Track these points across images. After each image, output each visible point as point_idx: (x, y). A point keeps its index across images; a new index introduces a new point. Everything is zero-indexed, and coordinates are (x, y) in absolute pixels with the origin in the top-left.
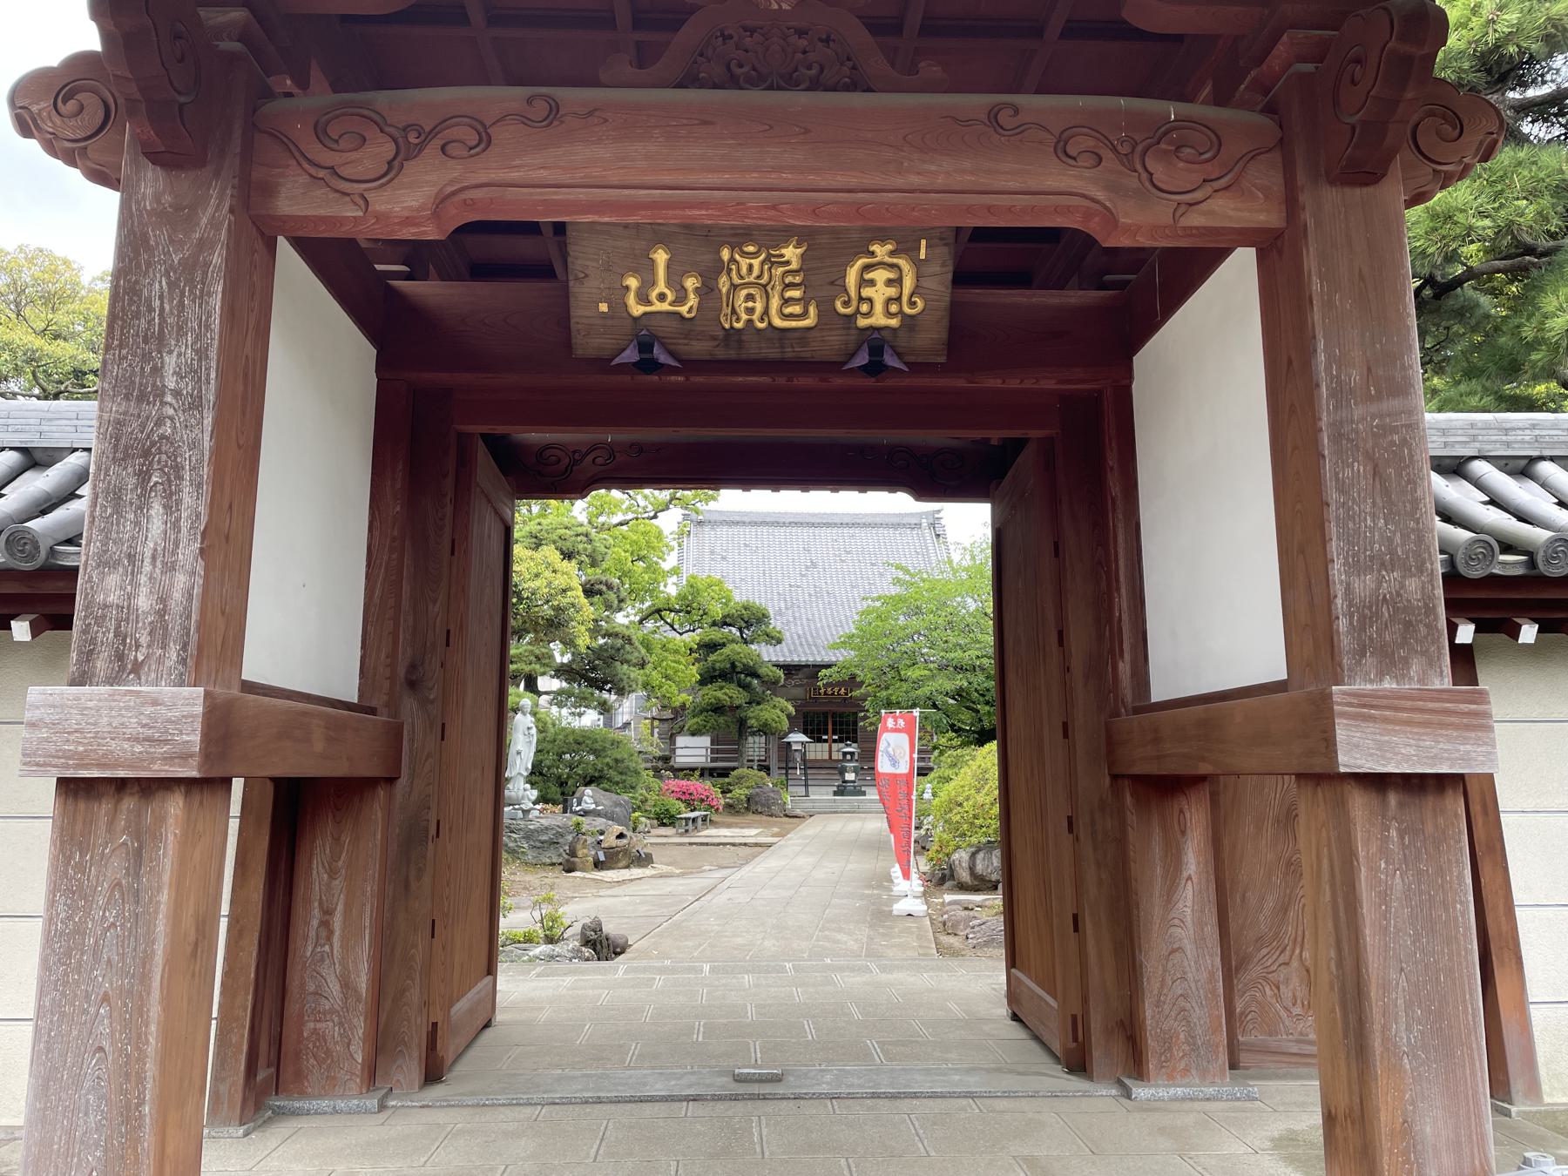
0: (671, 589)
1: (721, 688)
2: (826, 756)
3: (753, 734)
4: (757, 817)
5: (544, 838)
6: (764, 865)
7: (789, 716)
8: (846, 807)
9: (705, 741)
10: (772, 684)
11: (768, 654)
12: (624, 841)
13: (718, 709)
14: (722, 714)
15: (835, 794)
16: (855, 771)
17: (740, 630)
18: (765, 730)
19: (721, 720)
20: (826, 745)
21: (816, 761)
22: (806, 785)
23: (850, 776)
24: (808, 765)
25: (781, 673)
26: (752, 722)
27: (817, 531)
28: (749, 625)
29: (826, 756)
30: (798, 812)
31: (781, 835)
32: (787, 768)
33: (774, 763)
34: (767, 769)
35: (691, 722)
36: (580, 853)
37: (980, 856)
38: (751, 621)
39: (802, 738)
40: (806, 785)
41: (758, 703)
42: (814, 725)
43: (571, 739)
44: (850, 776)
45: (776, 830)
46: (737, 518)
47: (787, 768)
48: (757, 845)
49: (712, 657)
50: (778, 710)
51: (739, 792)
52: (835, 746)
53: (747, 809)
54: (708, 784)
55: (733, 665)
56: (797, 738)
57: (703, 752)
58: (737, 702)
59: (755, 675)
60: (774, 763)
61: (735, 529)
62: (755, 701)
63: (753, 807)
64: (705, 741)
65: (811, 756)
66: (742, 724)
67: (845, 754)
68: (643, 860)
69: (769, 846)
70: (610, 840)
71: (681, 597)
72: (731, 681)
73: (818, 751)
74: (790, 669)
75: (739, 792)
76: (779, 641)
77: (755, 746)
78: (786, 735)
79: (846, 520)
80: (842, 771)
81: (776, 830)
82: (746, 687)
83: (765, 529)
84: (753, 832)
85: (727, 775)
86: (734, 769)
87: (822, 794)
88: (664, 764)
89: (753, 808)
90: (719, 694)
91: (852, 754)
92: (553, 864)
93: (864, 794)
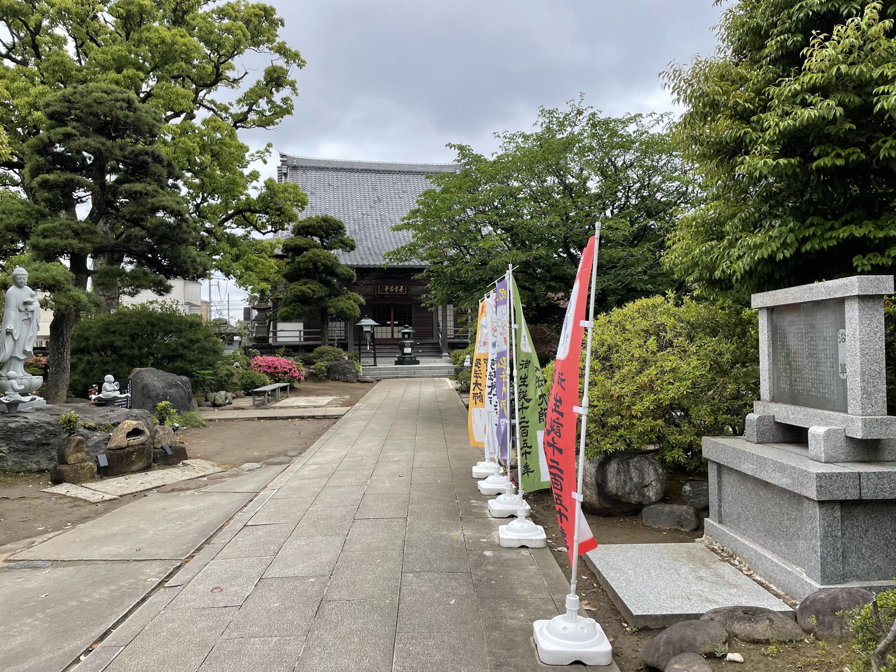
0: (254, 192)
1: (305, 284)
2: (389, 336)
3: (333, 320)
4: (335, 384)
5: (29, 438)
6: (327, 452)
7: (361, 306)
8: (405, 373)
9: (300, 326)
10: (346, 281)
11: (345, 259)
12: (141, 439)
13: (303, 299)
14: (309, 304)
15: (397, 363)
16: (412, 346)
17: (321, 238)
18: (341, 316)
19: (307, 308)
20: (389, 329)
21: (382, 339)
22: (375, 357)
23: (408, 350)
24: (375, 343)
25: (354, 273)
26: (332, 310)
27: (382, 176)
28: (328, 235)
29: (389, 336)
30: (368, 378)
31: (350, 404)
32: (360, 345)
33: (351, 342)
34: (345, 347)
35: (282, 310)
36: (72, 459)
37: (613, 467)
38: (329, 231)
39: (371, 322)
40: (375, 357)
41: (337, 296)
42: (380, 311)
43: (144, 322)
44: (408, 350)
45: (347, 397)
46: (323, 165)
47: (360, 345)
48: (324, 417)
49: (298, 259)
50: (352, 301)
51: (321, 364)
52: (396, 329)
53: (328, 377)
54: (291, 360)
55: (315, 264)
56: (367, 323)
57: (297, 334)
58: (319, 294)
59: (334, 274)
60: (351, 342)
61: (322, 173)
62: (335, 293)
63: (334, 375)
64: (300, 326)
65: (378, 336)
66: (324, 311)
67: (404, 334)
68: (174, 457)
69: (337, 418)
70: (119, 439)
71: (261, 198)
72: (314, 278)
73: (383, 333)
74: (363, 271)
75: (321, 364)
76: (353, 248)
77: (336, 329)
78: (359, 320)
79: (402, 170)
80: (402, 347)
81: (347, 397)
82: (327, 283)
83: (344, 174)
84: (324, 400)
85: (312, 351)
86: (316, 346)
87: (386, 364)
88: (263, 345)
89: (332, 376)
90: (304, 288)
91: (409, 333)
92: (41, 471)
93: (418, 363)
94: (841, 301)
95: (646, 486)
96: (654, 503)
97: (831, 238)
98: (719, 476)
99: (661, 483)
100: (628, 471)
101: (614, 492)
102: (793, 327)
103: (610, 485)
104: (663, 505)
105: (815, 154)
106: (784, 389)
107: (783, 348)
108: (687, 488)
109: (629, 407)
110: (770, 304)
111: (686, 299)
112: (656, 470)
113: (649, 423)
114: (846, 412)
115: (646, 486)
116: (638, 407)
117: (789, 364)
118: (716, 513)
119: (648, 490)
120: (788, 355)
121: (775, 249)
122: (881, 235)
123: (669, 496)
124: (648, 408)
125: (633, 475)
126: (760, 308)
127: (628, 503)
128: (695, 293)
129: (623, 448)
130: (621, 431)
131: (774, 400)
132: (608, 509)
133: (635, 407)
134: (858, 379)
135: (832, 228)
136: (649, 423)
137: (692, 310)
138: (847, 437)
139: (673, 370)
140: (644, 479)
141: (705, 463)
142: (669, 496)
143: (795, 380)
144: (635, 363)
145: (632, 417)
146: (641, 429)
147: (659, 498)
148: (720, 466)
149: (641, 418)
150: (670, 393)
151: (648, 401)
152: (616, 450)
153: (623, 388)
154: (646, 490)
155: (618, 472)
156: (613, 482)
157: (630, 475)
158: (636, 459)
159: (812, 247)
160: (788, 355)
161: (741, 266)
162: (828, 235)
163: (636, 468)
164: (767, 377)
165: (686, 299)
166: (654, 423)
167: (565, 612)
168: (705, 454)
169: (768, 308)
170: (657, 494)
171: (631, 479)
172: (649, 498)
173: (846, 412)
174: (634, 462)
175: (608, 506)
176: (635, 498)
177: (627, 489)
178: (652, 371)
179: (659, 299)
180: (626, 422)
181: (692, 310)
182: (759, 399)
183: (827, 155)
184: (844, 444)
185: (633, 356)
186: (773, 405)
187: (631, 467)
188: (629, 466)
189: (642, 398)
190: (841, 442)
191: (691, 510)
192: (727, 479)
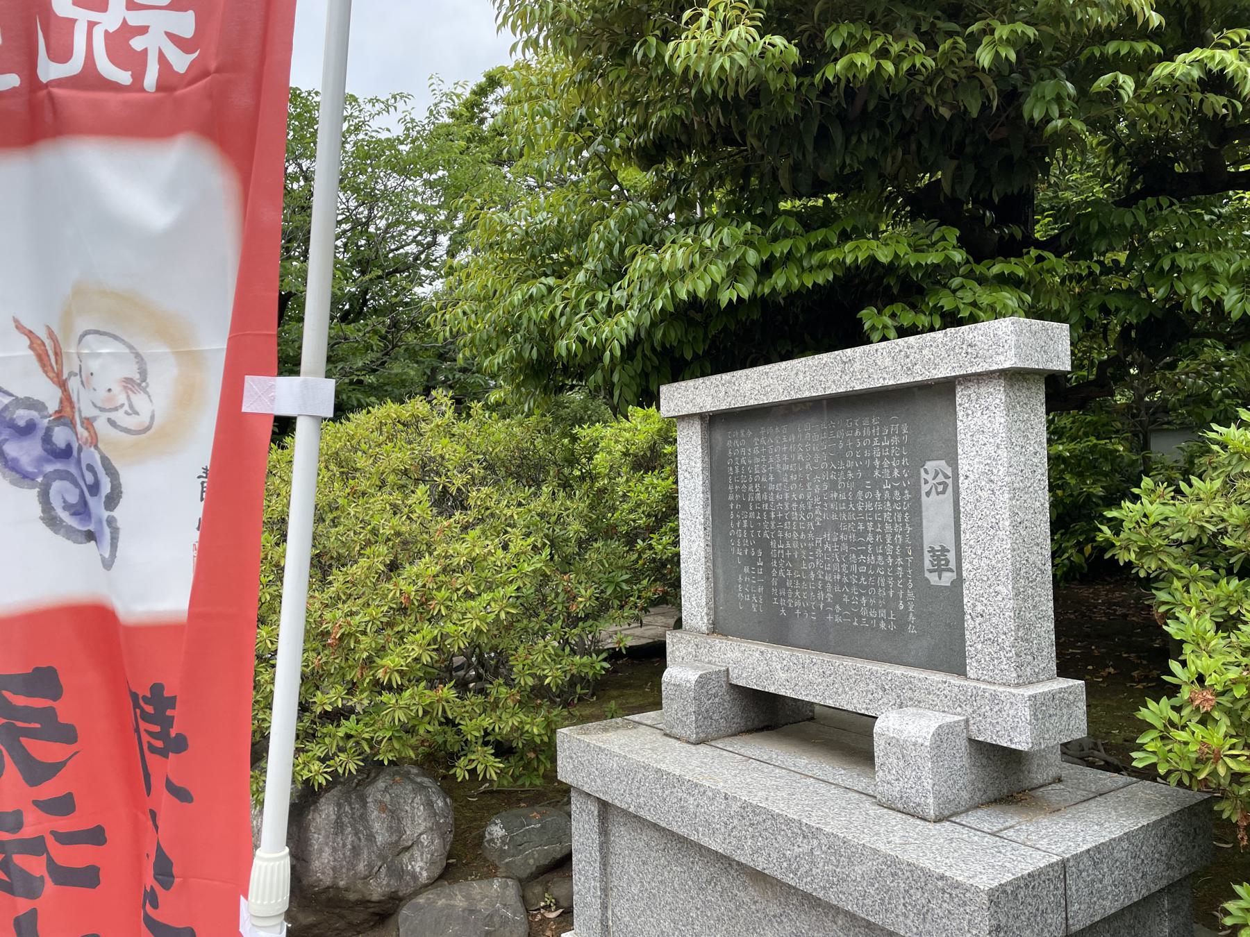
37: (324, 814)
94: (944, 390)
95: (407, 849)
96: (426, 886)
97: (822, 266)
98: (604, 832)
99: (442, 836)
100: (364, 817)
101: (328, 881)
102: (787, 459)
103: (316, 864)
104: (446, 888)
105: (837, 45)
106: (747, 605)
107: (745, 505)
108: (497, 831)
109: (369, 662)
110: (710, 405)
111: (476, 406)
112: (429, 804)
113: (415, 698)
114: (961, 672)
115: (407, 849)
116: (392, 661)
117: (763, 544)
118: (596, 924)
119: (412, 858)
120: (757, 525)
121: (718, 280)
122: (1079, 198)
123: (462, 859)
124: (417, 660)
125: (377, 826)
126: (682, 418)
127: (364, 903)
128: (493, 397)
129: (352, 767)
130: (348, 726)
131: (717, 628)
132: (314, 925)
133: (387, 661)
134: (1006, 590)
135: (825, 245)
136: (415, 698)
137: (501, 434)
138: (971, 741)
139: (472, 562)
140: (400, 832)
141: (559, 795)
142: (462, 859)
143: (782, 583)
144: (383, 549)
145: (379, 687)
146: (400, 715)
147: (437, 872)
148: (604, 806)
149: (400, 689)
150: (469, 619)
151: (416, 647)
152: (334, 774)
153: (352, 614)
154: (405, 857)
155: (339, 826)
156: (326, 856)
157: (368, 827)
158: (381, 784)
159: (788, 285)
160: (757, 525)
161: (618, 329)
162: (816, 259)
163: (383, 807)
164: (700, 576)
165: (476, 406)
166: (430, 696)
167: (297, 373)
168: (566, 771)
169: (701, 416)
170: (432, 863)
171: (371, 838)
172: (414, 876)
173: (961, 672)
174: (377, 790)
175: (311, 919)
176: (378, 889)
177: (361, 867)
178: (426, 567)
179: (418, 406)
180: (361, 701)
181: (501, 434)
182: (678, 625)
183: (862, 45)
184: (966, 761)
185: (375, 532)
186: (718, 642)
187: (371, 806)
188: (364, 804)
189: (401, 636)
190: (961, 758)
191: (512, 891)
192: (622, 837)
